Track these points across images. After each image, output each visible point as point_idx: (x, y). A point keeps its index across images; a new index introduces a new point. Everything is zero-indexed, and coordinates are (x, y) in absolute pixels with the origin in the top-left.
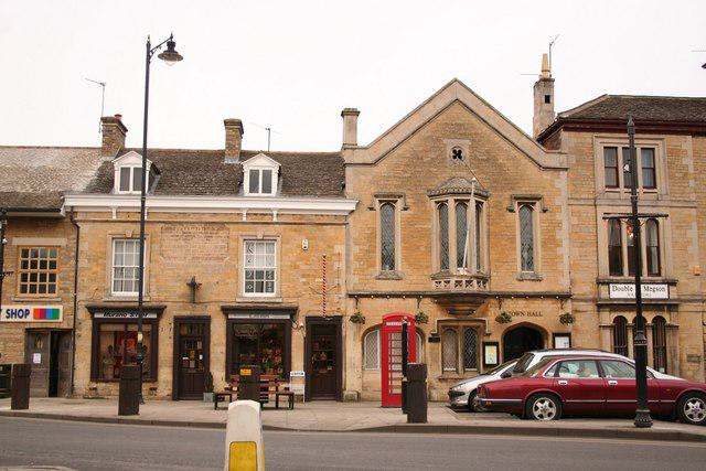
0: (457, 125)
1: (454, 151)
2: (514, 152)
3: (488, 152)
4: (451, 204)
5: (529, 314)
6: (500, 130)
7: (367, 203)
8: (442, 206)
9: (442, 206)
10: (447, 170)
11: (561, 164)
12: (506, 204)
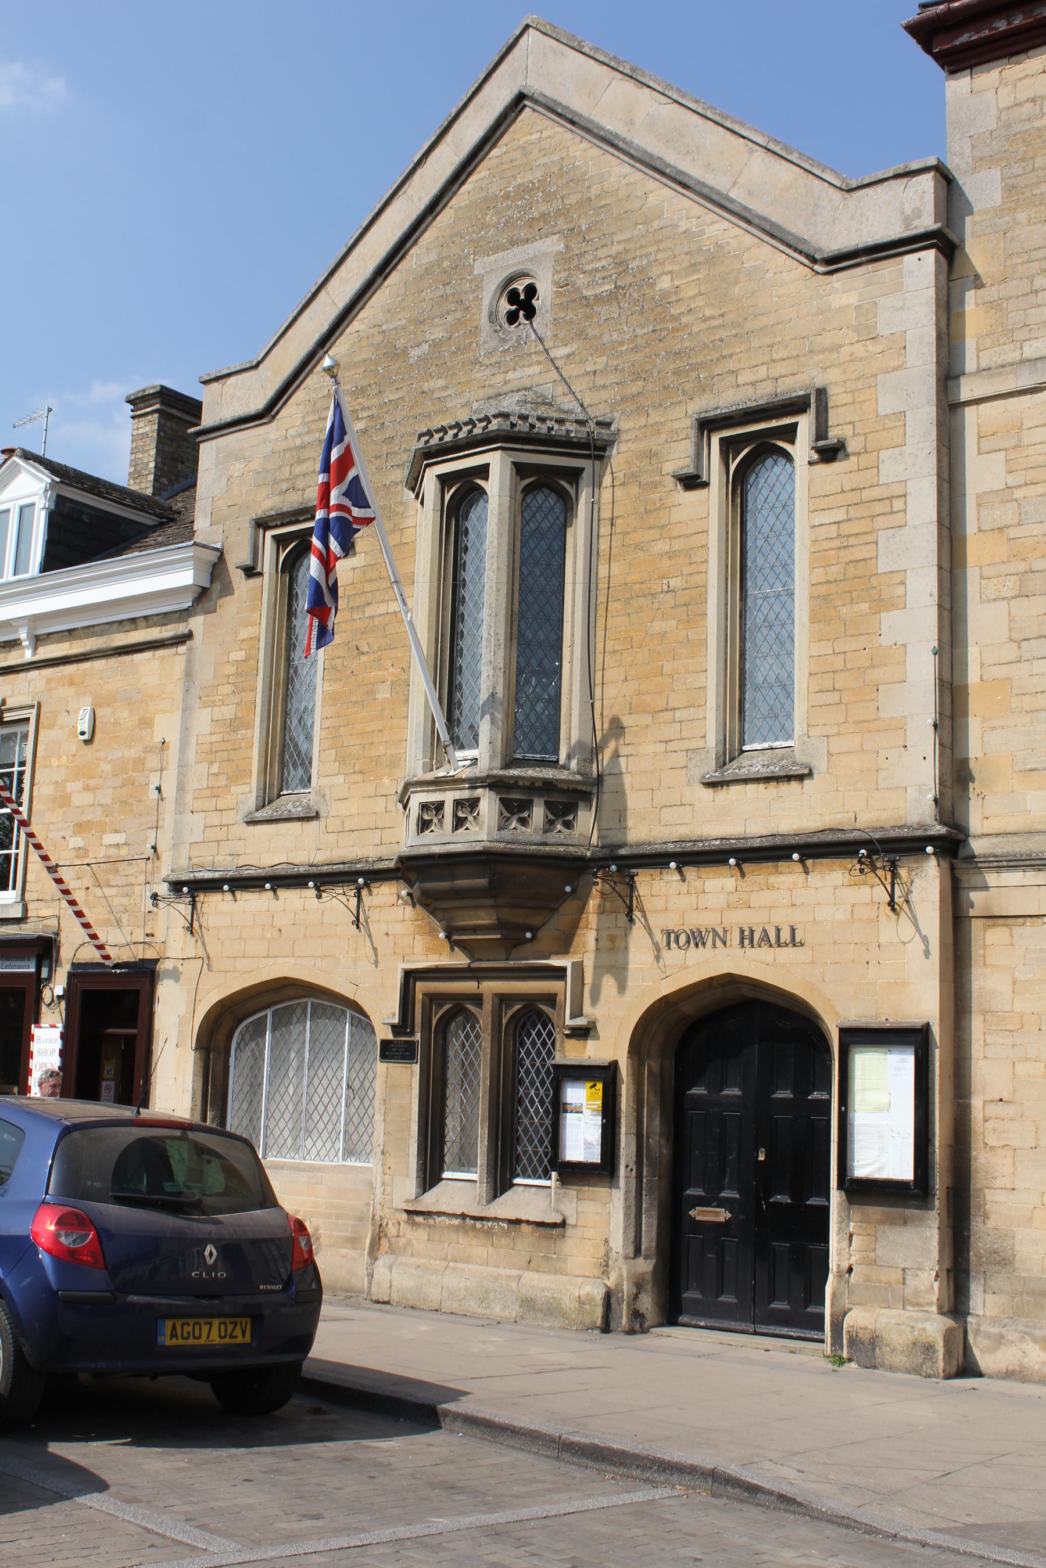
0: (525, 190)
1: (513, 297)
2: (720, 229)
3: (620, 263)
4: (498, 485)
5: (747, 938)
6: (673, 158)
7: (238, 556)
8: (463, 495)
9: (463, 495)
10: (479, 374)
11: (907, 221)
12: (680, 456)
